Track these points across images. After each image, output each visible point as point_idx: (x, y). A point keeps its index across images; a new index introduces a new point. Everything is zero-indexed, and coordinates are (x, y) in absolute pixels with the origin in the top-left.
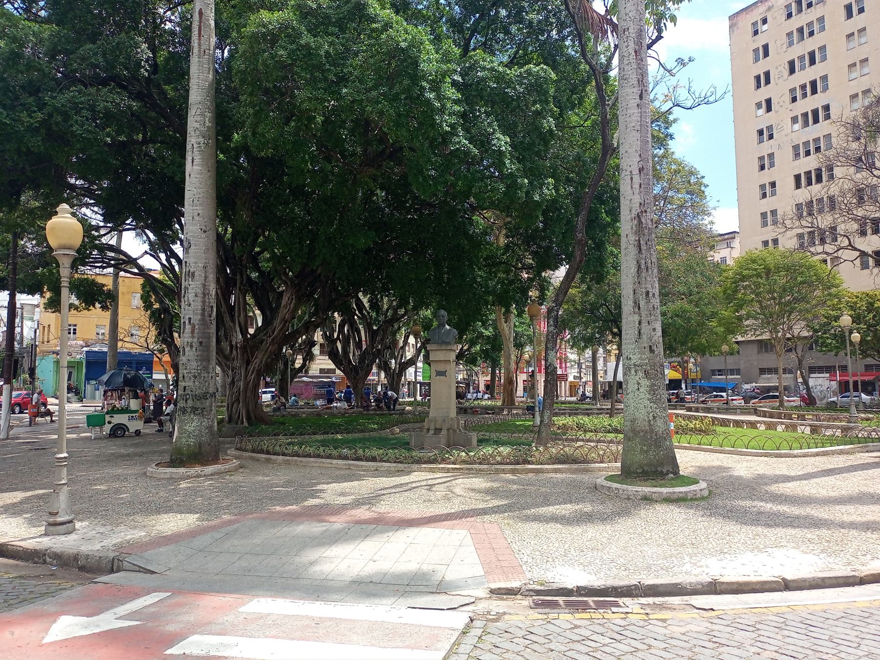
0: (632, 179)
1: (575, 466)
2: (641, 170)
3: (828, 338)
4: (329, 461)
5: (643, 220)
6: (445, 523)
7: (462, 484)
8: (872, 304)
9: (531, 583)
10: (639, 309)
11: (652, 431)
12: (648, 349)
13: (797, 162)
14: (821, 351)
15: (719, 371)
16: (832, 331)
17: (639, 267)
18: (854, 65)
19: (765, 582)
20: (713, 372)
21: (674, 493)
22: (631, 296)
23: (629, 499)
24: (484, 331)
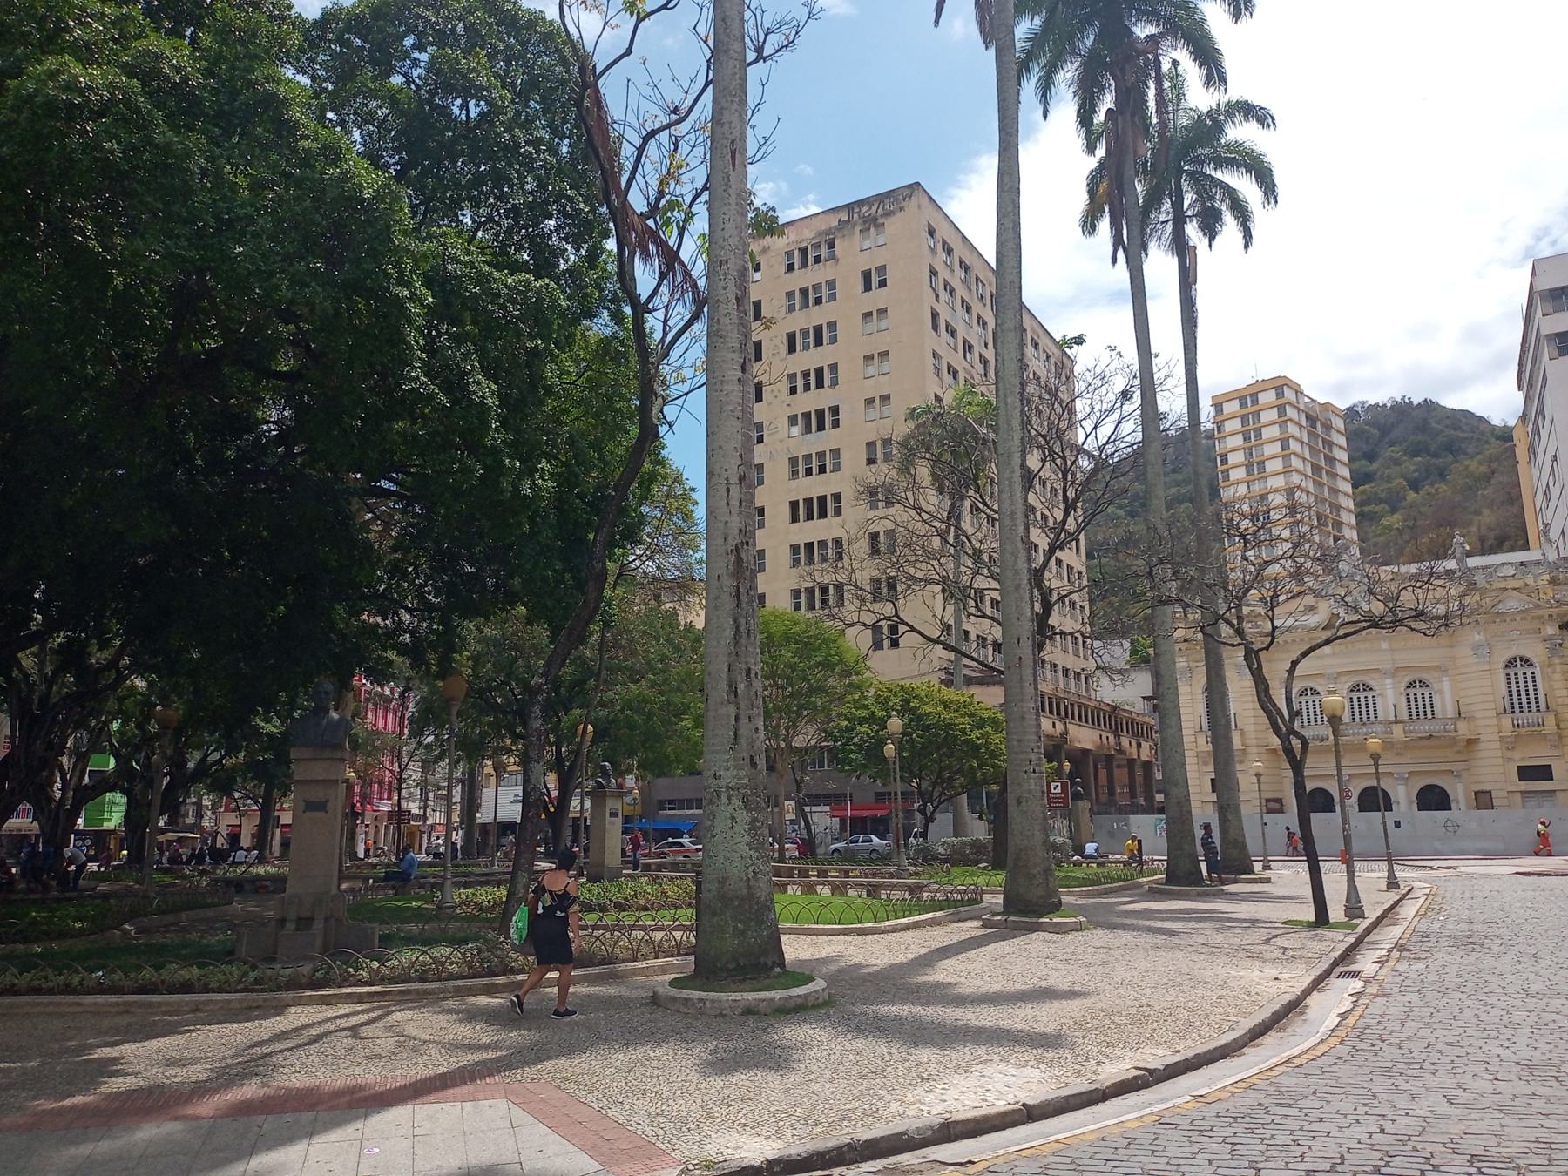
0: (728, 490)
1: (595, 970)
2: (742, 479)
3: (851, 751)
4: (71, 999)
5: (743, 556)
6: (451, 1091)
7: (419, 1022)
8: (907, 702)
9: (691, 1167)
10: (736, 695)
11: (751, 896)
12: (748, 761)
13: (794, 483)
14: (843, 771)
15: (671, 802)
16: (856, 740)
17: (738, 629)
18: (871, 357)
19: (1006, 1113)
20: (662, 805)
21: (791, 997)
22: (724, 675)
23: (722, 1015)
24: (262, 724)
